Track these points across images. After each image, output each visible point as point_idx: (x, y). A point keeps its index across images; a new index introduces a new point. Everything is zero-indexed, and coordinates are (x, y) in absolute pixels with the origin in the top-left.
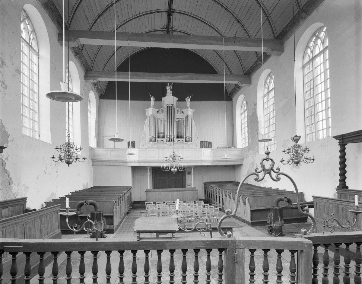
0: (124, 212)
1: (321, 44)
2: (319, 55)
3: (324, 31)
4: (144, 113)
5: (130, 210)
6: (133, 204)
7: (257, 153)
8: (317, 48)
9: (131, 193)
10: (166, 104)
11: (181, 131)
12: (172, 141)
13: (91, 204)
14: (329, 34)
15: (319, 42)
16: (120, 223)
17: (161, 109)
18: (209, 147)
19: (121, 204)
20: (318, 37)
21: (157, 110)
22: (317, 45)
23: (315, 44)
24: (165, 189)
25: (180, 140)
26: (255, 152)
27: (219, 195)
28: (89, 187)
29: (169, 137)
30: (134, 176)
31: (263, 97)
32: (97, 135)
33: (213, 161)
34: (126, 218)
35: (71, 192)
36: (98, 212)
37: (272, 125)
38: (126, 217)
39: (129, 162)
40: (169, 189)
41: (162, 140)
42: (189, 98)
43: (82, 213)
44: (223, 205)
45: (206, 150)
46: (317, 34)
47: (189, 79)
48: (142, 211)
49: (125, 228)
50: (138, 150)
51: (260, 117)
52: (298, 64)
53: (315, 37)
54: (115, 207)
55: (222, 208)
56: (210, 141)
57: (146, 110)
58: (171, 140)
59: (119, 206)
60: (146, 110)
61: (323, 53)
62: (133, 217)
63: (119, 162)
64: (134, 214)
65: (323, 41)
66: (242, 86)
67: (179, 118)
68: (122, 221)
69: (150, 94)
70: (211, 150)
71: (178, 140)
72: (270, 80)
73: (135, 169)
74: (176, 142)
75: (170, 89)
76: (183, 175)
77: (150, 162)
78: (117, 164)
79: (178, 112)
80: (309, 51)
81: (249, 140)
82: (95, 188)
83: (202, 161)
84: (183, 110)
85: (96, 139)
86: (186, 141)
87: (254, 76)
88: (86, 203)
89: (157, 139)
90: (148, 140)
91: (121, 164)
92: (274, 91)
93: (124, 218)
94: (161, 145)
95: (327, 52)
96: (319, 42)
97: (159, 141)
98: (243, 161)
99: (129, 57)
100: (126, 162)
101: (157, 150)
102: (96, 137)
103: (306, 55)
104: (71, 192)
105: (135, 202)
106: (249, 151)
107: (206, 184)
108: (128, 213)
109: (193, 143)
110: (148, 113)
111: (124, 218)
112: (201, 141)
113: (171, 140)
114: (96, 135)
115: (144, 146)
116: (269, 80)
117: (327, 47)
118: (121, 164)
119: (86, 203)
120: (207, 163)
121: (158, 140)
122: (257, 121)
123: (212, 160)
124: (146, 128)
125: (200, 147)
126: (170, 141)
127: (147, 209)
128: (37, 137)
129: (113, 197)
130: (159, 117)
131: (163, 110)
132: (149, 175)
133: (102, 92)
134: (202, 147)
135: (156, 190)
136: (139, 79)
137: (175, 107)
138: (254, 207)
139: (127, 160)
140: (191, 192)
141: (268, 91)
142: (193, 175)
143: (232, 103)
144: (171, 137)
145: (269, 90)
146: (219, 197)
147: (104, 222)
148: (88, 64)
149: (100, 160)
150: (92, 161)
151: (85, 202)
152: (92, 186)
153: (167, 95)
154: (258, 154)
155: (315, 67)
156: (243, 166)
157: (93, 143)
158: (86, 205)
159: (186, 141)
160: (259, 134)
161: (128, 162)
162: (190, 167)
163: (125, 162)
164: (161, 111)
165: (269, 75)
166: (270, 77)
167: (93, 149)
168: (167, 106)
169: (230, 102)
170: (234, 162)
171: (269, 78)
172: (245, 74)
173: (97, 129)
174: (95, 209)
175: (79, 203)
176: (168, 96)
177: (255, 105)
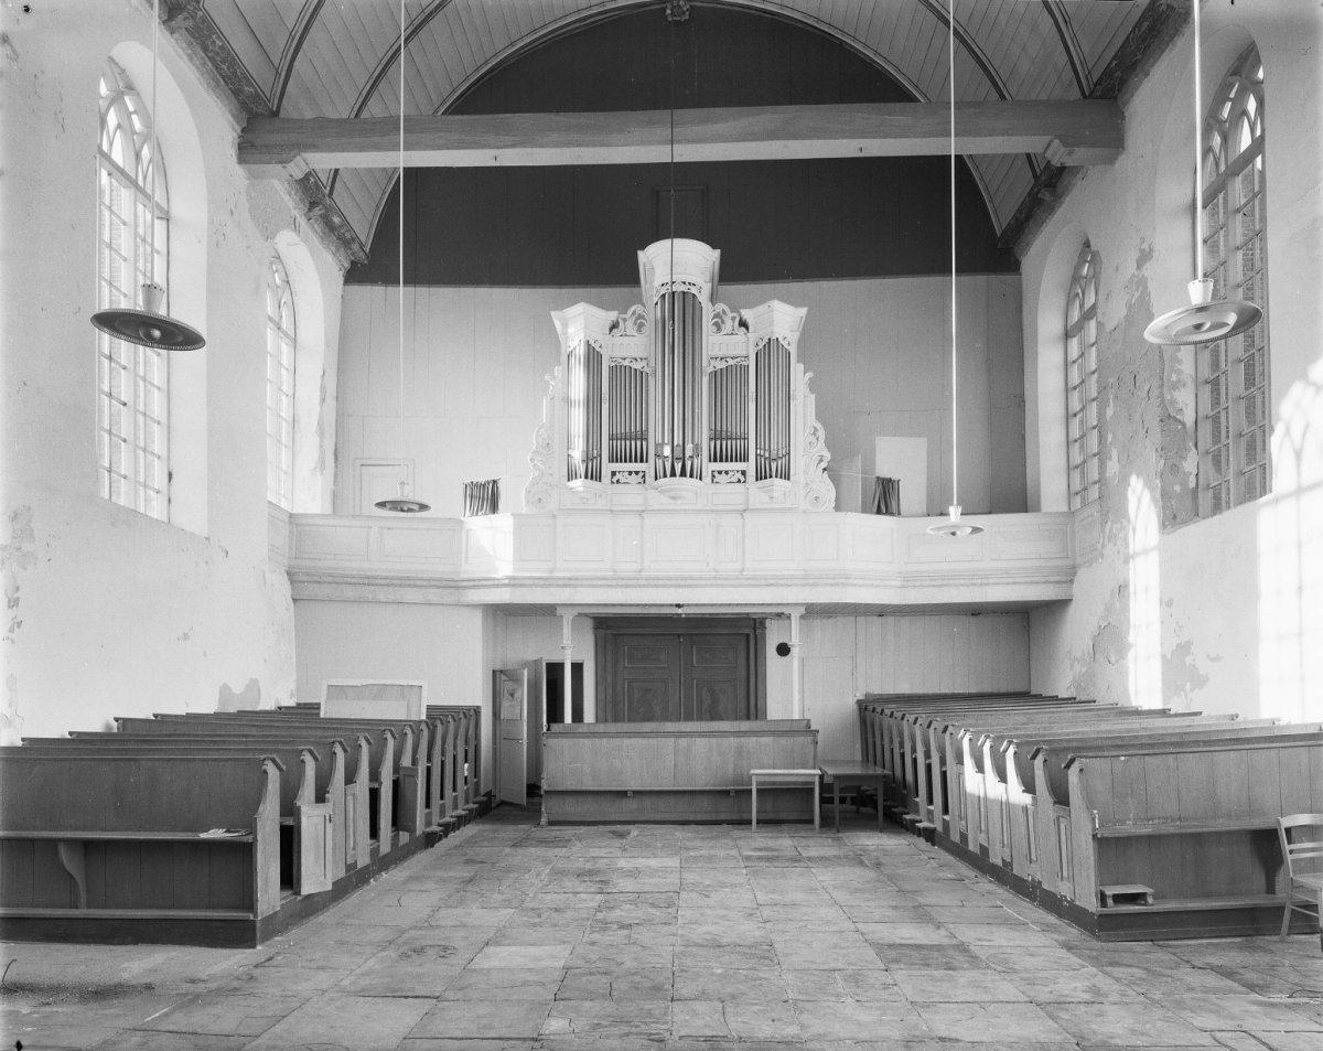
4: (553, 341)
10: (657, 283)
12: (683, 474)
21: (613, 315)
25: (727, 473)
27: (928, 755)
28: (267, 704)
29: (667, 451)
35: (117, 720)
41: (637, 473)
44: (946, 810)
47: (772, 135)
55: (940, 828)
58: (682, 468)
63: (418, 583)
67: (721, 354)
71: (720, 472)
77: (568, 583)
79: (718, 327)
84: (747, 314)
89: (607, 467)
97: (618, 476)
98: (1072, 581)
104: (117, 720)
106: (1103, 526)
121: (614, 474)
126: (673, 474)
128: (157, 510)
131: (640, 317)
133: (355, 247)
136: (507, 147)
137: (703, 298)
139: (462, 576)
140: (783, 741)
143: (1020, 281)
146: (929, 768)
148: (247, 79)
156: (1072, 608)
161: (465, 587)
163: (454, 585)
164: (630, 323)
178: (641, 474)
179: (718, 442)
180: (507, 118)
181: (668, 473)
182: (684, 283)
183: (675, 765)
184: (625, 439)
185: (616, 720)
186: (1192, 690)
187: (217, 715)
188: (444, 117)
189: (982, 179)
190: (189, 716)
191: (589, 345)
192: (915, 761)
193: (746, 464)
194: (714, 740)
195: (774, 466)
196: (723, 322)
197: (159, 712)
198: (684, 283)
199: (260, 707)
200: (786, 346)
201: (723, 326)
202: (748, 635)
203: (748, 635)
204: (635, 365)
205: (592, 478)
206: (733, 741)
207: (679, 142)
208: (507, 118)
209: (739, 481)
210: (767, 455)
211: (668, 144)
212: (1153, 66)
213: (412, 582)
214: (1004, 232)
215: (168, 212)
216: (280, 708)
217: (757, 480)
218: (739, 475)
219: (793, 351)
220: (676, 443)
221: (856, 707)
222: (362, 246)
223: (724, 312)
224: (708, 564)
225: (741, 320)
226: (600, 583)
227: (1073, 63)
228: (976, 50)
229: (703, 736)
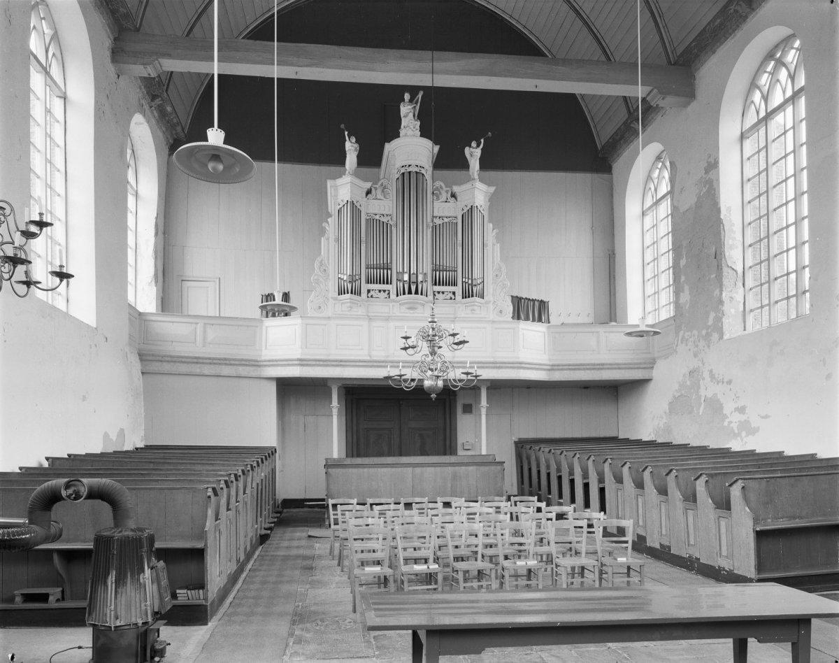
0: (250, 535)
1: (789, 80)
2: (780, 108)
5: (270, 529)
6: (280, 509)
7: (715, 336)
8: (778, 88)
9: (273, 471)
10: (398, 164)
11: (447, 262)
12: (416, 293)
13: (94, 494)
14: (806, 56)
15: (783, 74)
16: (233, 579)
17: (380, 183)
18: (540, 320)
19: (241, 505)
20: (780, 63)
21: (368, 185)
23: (775, 80)
24: (390, 460)
25: (443, 293)
26: (704, 332)
28: (128, 447)
29: (406, 277)
30: (282, 422)
31: (743, 137)
32: (160, 274)
33: (553, 368)
34: (255, 557)
35: (47, 459)
36: (130, 534)
37: (663, 289)
38: (257, 553)
39: (269, 366)
40: (405, 460)
41: (384, 291)
42: (478, 146)
43: (56, 538)
45: (530, 328)
46: (778, 55)
47: (481, 73)
48: (314, 532)
49: (254, 598)
50: (299, 321)
51: (729, 209)
52: (729, 129)
53: (773, 63)
54: (210, 512)
56: (545, 300)
57: (329, 183)
58: (412, 288)
59: (228, 509)
60: (329, 183)
61: (793, 104)
62: (281, 553)
64: (286, 544)
65: (765, 93)
66: (661, 103)
68: (240, 569)
69: (342, 126)
70: (548, 327)
71: (439, 292)
72: (660, 169)
73: (290, 390)
74: (431, 297)
75: (411, 115)
76: (448, 416)
78: (226, 370)
80: (757, 96)
81: (677, 293)
82: (148, 448)
83: (520, 365)
84: (456, 189)
85: (155, 288)
87: (708, 71)
88: (70, 491)
89: (365, 287)
90: (333, 288)
91: (243, 371)
92: (669, 200)
93: (249, 556)
94: (380, 306)
95: (803, 101)
96: (783, 74)
97: (372, 293)
99: (273, 15)
100: (259, 366)
102: (156, 282)
103: (647, 193)
104: (47, 459)
105: (288, 503)
107: (521, 445)
108: (263, 539)
109: (487, 303)
110: (336, 196)
111: (249, 556)
112: (515, 295)
113: (413, 288)
114: (156, 275)
115: (320, 307)
116: (658, 170)
117: (802, 89)
118: (243, 371)
119: (70, 491)
120: (535, 372)
121: (369, 291)
122: (719, 222)
123: (551, 363)
124: (328, 246)
125: (513, 318)
126: (410, 292)
127: (336, 523)
129: (207, 476)
130: (371, 211)
132: (335, 412)
133: (179, 129)
134: (517, 315)
135: (359, 461)
136: (307, 66)
137: (428, 176)
138: (764, 519)
139: (263, 358)
141: (655, 200)
142: (484, 411)
143: (612, 178)
145: (658, 198)
147: (156, 580)
149: (171, 357)
150: (141, 360)
151: (67, 486)
152: (141, 445)
153: (402, 132)
154: (721, 337)
155: (773, 139)
156: (652, 385)
157: (144, 297)
158: (69, 497)
160: (725, 269)
162: (473, 388)
163: (256, 364)
164: (379, 192)
165: (659, 158)
166: (661, 164)
167: (144, 317)
169: (606, 176)
170: (623, 371)
171: (659, 167)
172: (669, 63)
173: (161, 255)
174: (115, 518)
175: (39, 488)
176: (406, 135)
177: (713, 165)
178: (387, 292)
179: (438, 273)
180: (304, 47)
182: (417, 166)
183: (413, 487)
184: (377, 269)
185: (359, 456)
186: (747, 436)
187: (102, 455)
188: (243, 40)
189: (589, 112)
190: (87, 455)
191: (353, 204)
192: (572, 482)
193: (391, 286)
194: (438, 469)
195: (475, 289)
196: (440, 193)
197: (70, 453)
198: (417, 166)
199: (125, 448)
200: (358, 207)
201: (440, 197)
202: (445, 399)
203: (445, 399)
205: (355, 294)
206: (450, 469)
207: (437, 73)
208: (304, 47)
209: (451, 298)
210: (470, 282)
211: (427, 73)
212: (717, 48)
213: (228, 362)
214: (603, 147)
215: (65, 93)
216: (137, 449)
217: (463, 298)
218: (451, 295)
219: (486, 214)
220: (412, 272)
221: (513, 445)
222: (183, 130)
223: (441, 187)
225: (452, 193)
226: (361, 364)
227: (664, 43)
228: (595, 30)
229: (432, 466)
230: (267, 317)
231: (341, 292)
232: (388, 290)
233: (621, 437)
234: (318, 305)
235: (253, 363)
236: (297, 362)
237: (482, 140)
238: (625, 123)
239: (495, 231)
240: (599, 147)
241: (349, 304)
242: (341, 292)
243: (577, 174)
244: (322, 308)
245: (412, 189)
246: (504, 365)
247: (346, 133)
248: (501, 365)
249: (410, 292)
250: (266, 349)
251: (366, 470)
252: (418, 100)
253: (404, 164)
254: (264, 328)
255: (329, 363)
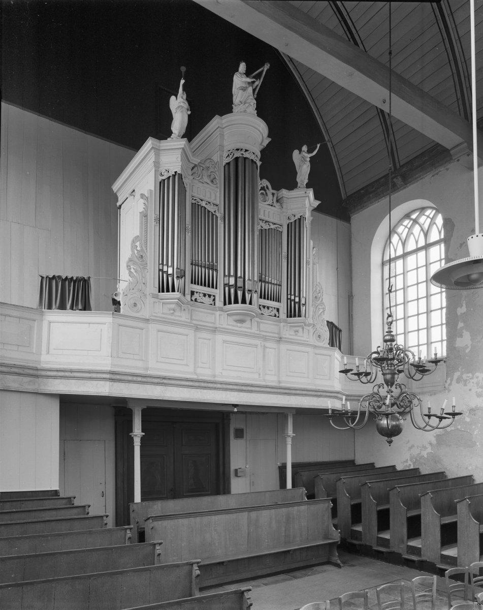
3: (411, 219)
15: (417, 229)
22: (435, 225)
25: (268, 308)
29: (232, 281)
39: (55, 377)
41: (210, 296)
67: (267, 219)
71: (264, 307)
86: (290, 315)
97: (196, 296)
100: (37, 376)
101: (191, 332)
115: (135, 305)
121: (192, 293)
126: (236, 302)
142: (289, 441)
144: (240, 284)
159: (290, 315)
163: (34, 373)
168: (238, 154)
181: (240, 300)
204: (209, 208)
210: (297, 299)
218: (275, 311)
224: (260, 374)
226: (187, 383)
230: (50, 307)
231: (165, 287)
232: (214, 296)
233: (360, 460)
234: (132, 302)
235: (31, 372)
236: (108, 376)
237: (318, 145)
238: (386, 176)
239: (315, 249)
240: (344, 197)
241: (173, 306)
242: (165, 287)
243: (327, 217)
244: (138, 305)
245: (247, 180)
246: (324, 394)
247: (182, 82)
248: (322, 393)
249: (244, 301)
250: (48, 353)
251: (198, 519)
252: (261, 73)
253: (239, 146)
254: (45, 325)
255: (149, 380)
